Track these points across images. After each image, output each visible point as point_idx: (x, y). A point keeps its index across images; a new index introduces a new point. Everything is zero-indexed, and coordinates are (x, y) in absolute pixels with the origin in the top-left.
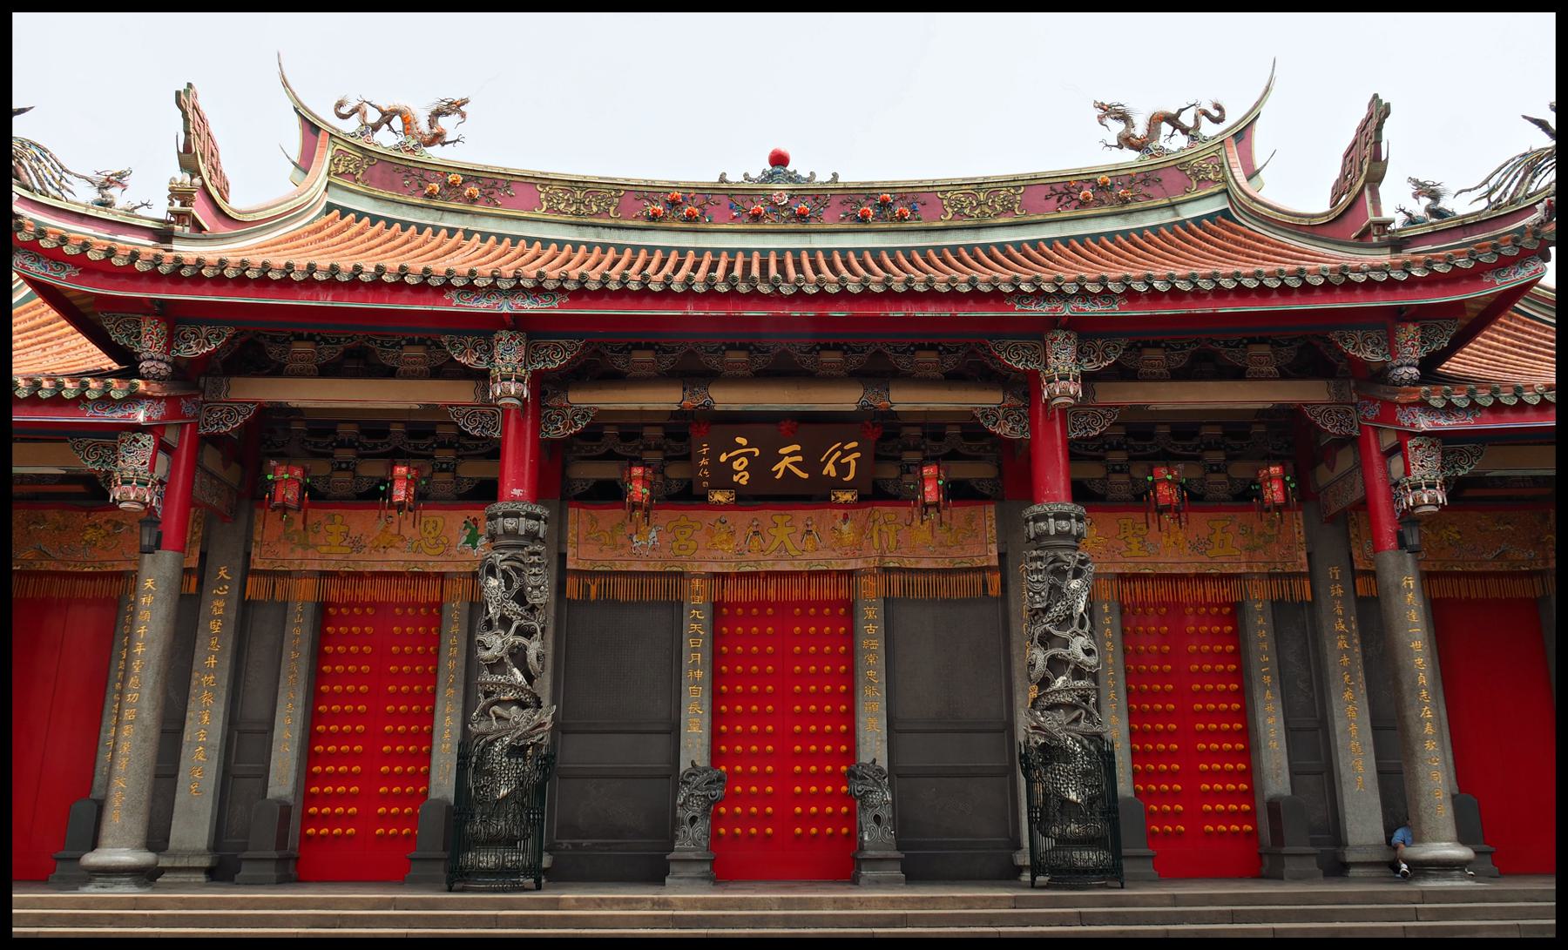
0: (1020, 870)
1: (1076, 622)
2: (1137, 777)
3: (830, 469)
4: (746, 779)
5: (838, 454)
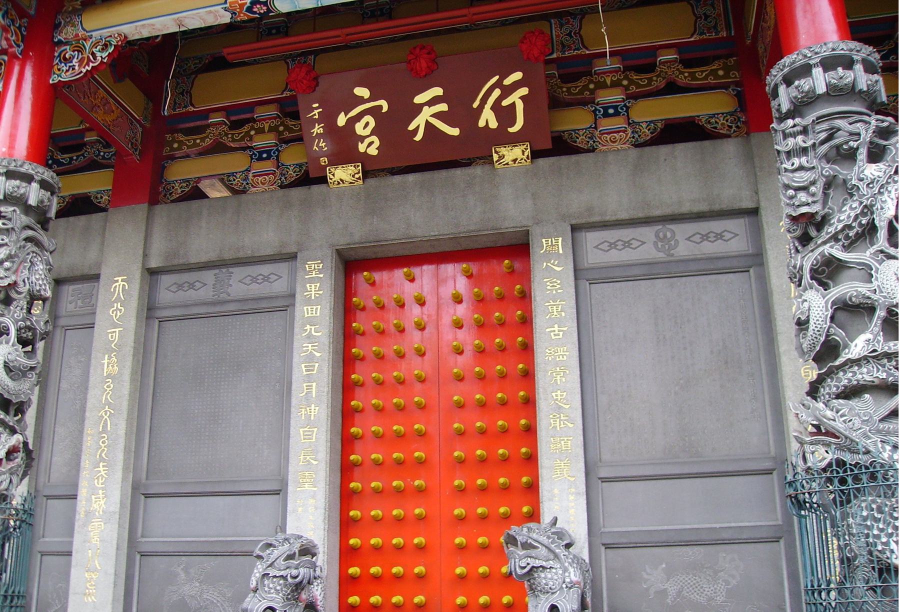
1: (882, 234)
3: (488, 118)
5: (497, 93)
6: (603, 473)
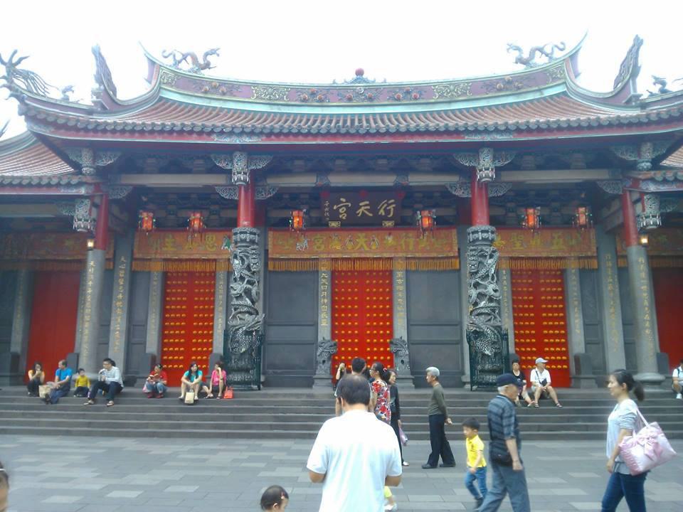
0: (465, 383)
1: (490, 278)
2: (517, 345)
3: (382, 212)
4: (346, 345)
5: (385, 205)
6: (412, 323)
